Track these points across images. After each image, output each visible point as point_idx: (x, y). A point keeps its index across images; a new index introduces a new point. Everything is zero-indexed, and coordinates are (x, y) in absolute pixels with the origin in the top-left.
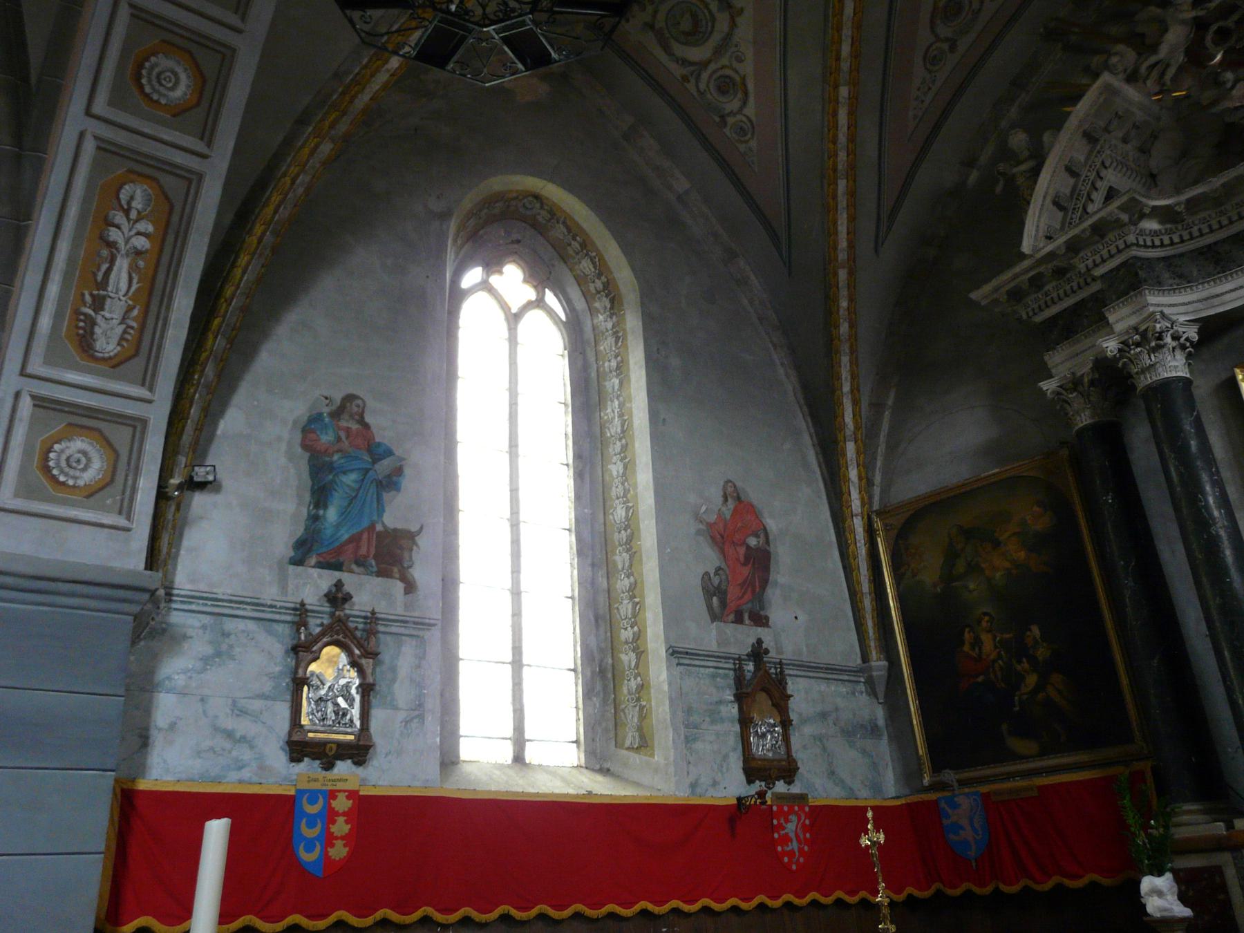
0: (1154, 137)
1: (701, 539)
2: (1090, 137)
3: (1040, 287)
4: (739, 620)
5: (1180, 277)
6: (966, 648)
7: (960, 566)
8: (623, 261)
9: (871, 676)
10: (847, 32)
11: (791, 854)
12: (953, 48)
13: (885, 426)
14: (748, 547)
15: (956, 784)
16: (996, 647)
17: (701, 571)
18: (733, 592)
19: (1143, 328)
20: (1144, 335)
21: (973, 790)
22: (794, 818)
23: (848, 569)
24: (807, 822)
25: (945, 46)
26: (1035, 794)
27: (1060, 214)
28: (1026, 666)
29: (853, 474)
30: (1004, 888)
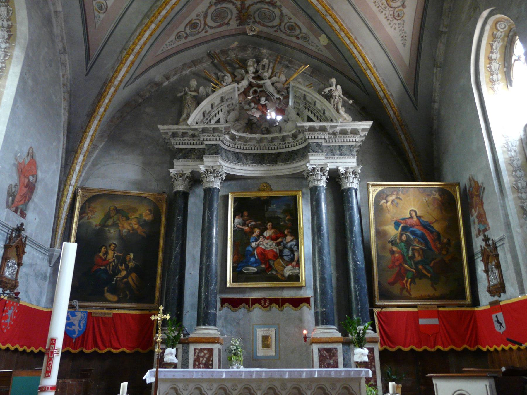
0: (233, 110)
1: (14, 168)
2: (222, 100)
3: (183, 137)
4: (16, 212)
5: (227, 157)
6: (101, 254)
7: (110, 222)
8: (26, 22)
9: (53, 254)
10: (168, 7)
11: (6, 324)
12: (186, 38)
13: (94, 155)
14: (29, 181)
15: (77, 307)
16: (114, 257)
17: (10, 182)
18: (18, 198)
19: (214, 168)
20: (214, 170)
21: (85, 310)
22: (12, 308)
23: (59, 206)
24: (17, 311)
25: (185, 35)
26: (111, 316)
27: (202, 117)
28: (123, 267)
29: (78, 168)
30: (85, 351)
